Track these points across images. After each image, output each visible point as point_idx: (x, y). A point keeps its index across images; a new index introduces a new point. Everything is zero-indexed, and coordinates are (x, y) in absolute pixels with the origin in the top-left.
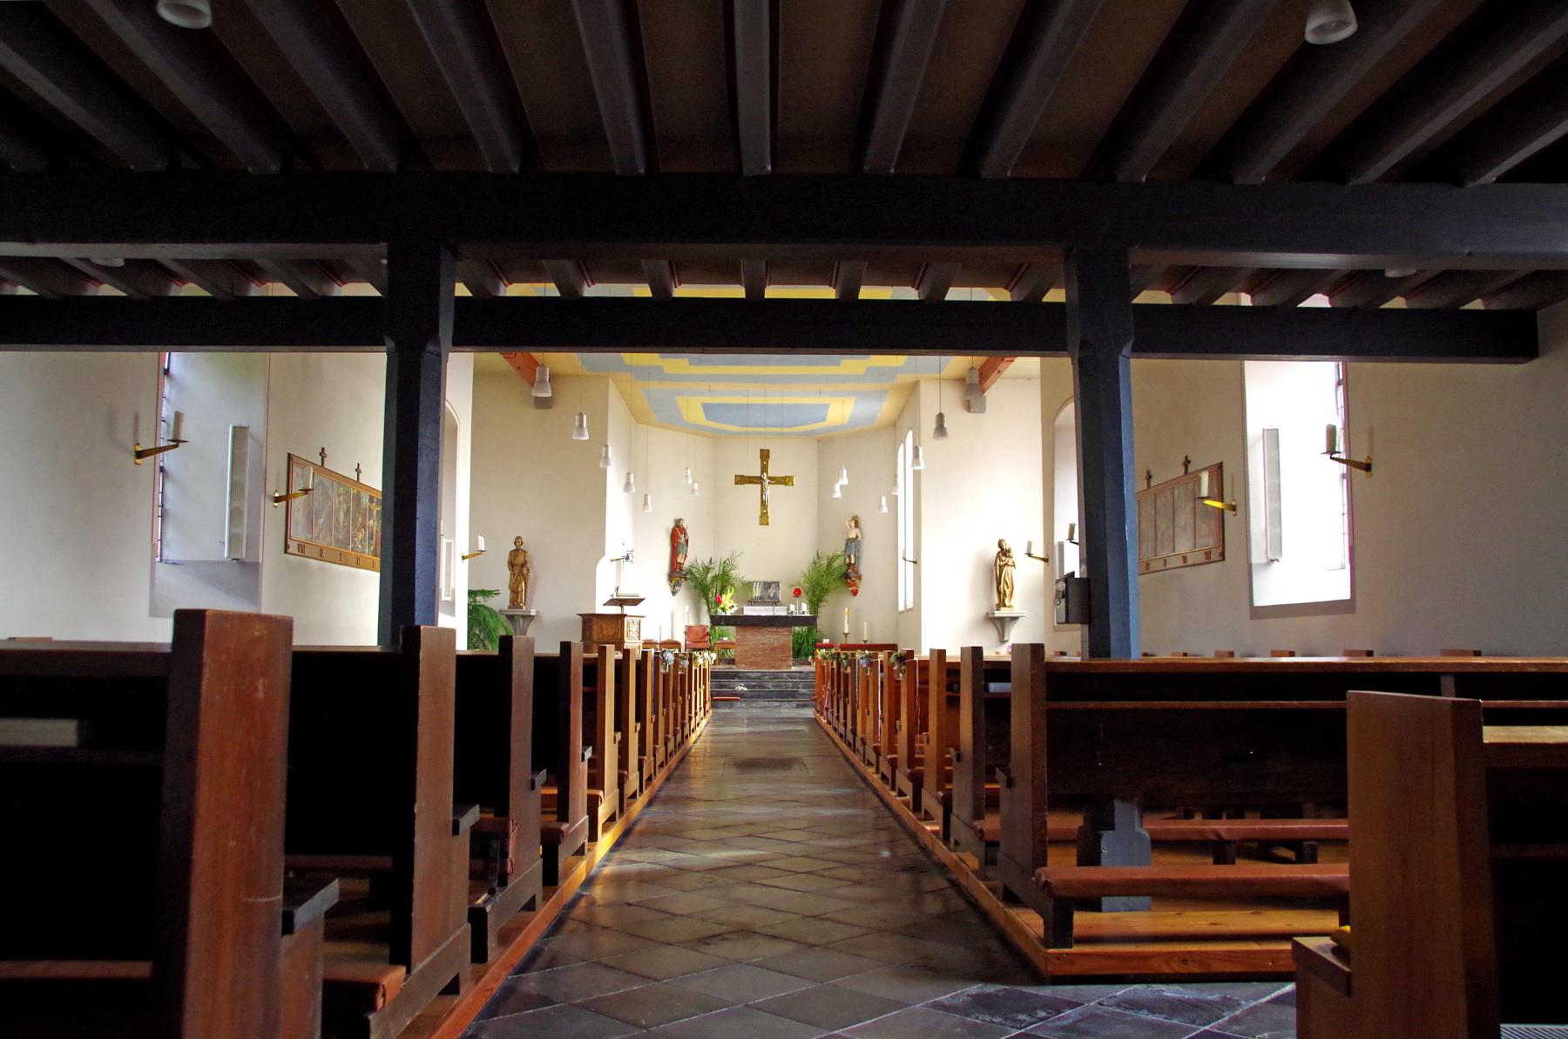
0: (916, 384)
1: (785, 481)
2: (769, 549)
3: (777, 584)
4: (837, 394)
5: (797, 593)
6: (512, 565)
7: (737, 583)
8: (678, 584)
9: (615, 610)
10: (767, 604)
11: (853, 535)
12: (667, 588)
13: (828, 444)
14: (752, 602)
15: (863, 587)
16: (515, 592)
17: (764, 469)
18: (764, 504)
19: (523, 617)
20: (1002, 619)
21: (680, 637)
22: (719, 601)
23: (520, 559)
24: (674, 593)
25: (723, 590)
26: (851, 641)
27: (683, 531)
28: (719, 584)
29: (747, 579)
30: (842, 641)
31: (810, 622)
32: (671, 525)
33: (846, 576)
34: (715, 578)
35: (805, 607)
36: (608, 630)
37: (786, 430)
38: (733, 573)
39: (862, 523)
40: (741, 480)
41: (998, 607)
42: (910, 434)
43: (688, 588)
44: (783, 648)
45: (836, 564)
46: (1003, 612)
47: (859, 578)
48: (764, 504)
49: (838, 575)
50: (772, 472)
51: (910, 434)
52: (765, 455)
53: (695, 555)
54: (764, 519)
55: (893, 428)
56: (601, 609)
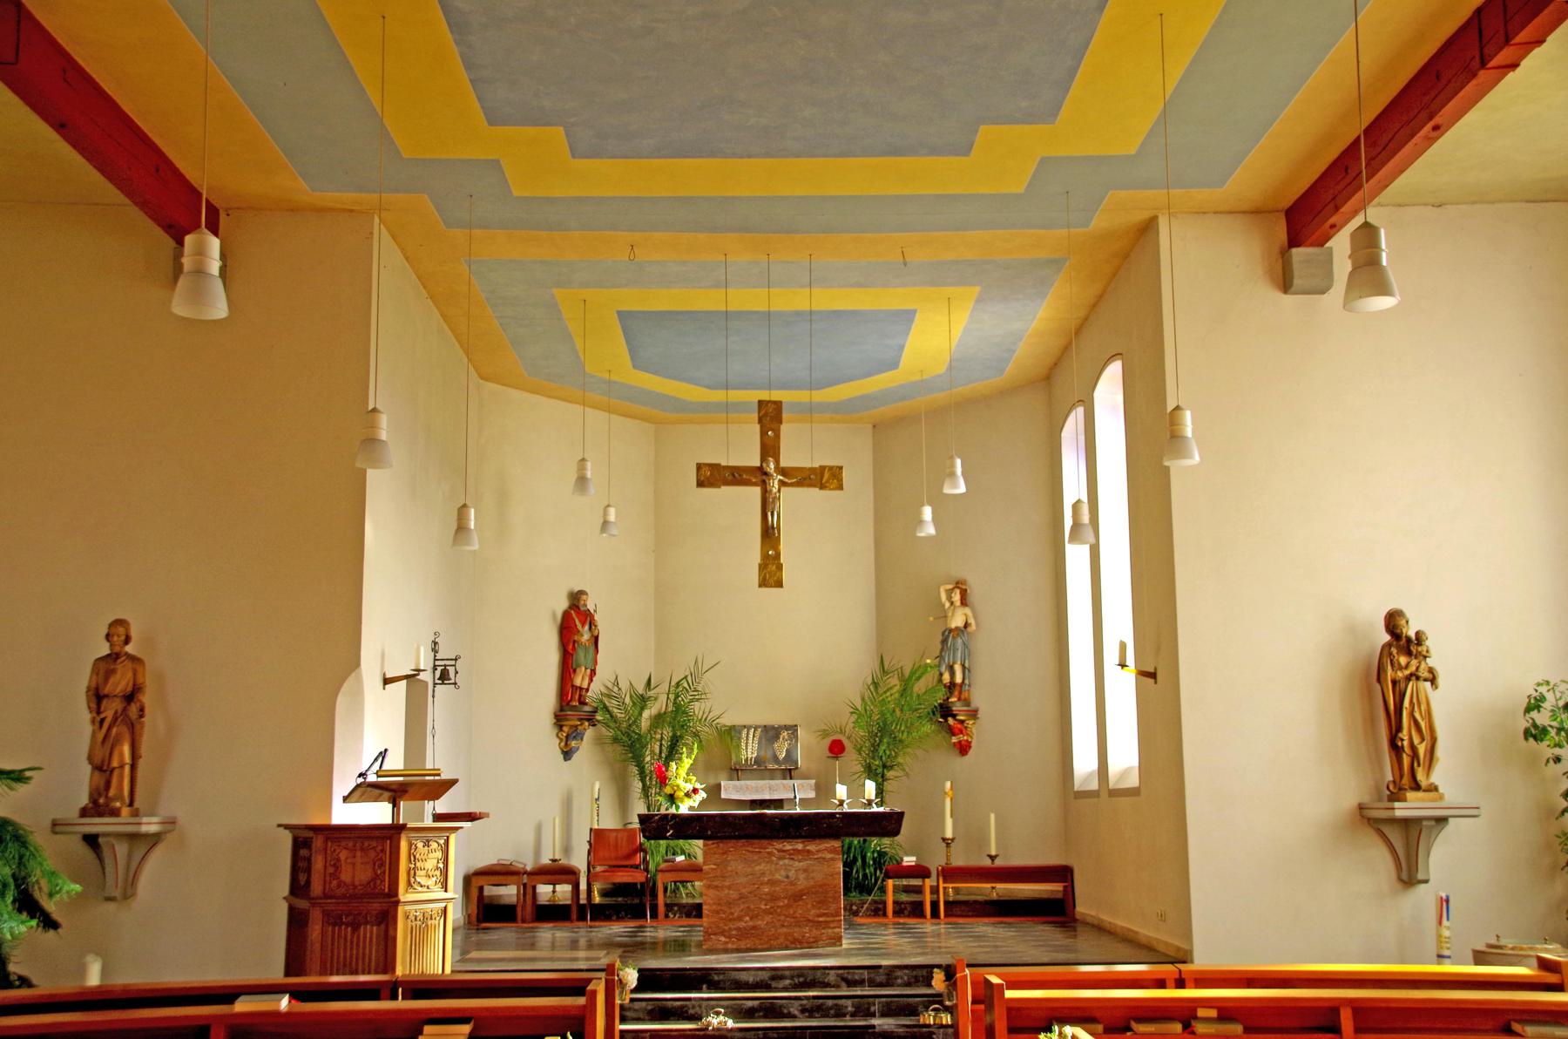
0: (1147, 228)
1: (824, 478)
2: (781, 645)
3: (793, 729)
4: (941, 275)
5: (837, 749)
6: (97, 697)
7: (705, 730)
8: (575, 734)
9: (377, 813)
10: (772, 774)
11: (957, 621)
12: (550, 743)
13: (907, 431)
14: (736, 772)
15: (977, 733)
16: (102, 768)
17: (769, 449)
18: (769, 534)
19: (134, 837)
20: (1406, 823)
21: (579, 861)
22: (663, 780)
23: (120, 682)
24: (567, 754)
25: (672, 753)
26: (958, 861)
27: (588, 618)
28: (667, 733)
29: (727, 721)
30: (935, 862)
31: (888, 824)
32: (562, 604)
33: (945, 711)
34: (658, 720)
35: (870, 787)
36: (356, 871)
37: (820, 396)
38: (697, 708)
39: (973, 596)
40: (712, 476)
41: (1396, 795)
42: (1109, 392)
43: (599, 741)
44: (820, 894)
45: (919, 687)
46: (1411, 806)
47: (974, 714)
48: (769, 534)
49: (926, 706)
50: (791, 501)
51: (1109, 392)
52: (770, 415)
53: (617, 665)
54: (770, 574)
55: (1054, 385)
56: (345, 814)
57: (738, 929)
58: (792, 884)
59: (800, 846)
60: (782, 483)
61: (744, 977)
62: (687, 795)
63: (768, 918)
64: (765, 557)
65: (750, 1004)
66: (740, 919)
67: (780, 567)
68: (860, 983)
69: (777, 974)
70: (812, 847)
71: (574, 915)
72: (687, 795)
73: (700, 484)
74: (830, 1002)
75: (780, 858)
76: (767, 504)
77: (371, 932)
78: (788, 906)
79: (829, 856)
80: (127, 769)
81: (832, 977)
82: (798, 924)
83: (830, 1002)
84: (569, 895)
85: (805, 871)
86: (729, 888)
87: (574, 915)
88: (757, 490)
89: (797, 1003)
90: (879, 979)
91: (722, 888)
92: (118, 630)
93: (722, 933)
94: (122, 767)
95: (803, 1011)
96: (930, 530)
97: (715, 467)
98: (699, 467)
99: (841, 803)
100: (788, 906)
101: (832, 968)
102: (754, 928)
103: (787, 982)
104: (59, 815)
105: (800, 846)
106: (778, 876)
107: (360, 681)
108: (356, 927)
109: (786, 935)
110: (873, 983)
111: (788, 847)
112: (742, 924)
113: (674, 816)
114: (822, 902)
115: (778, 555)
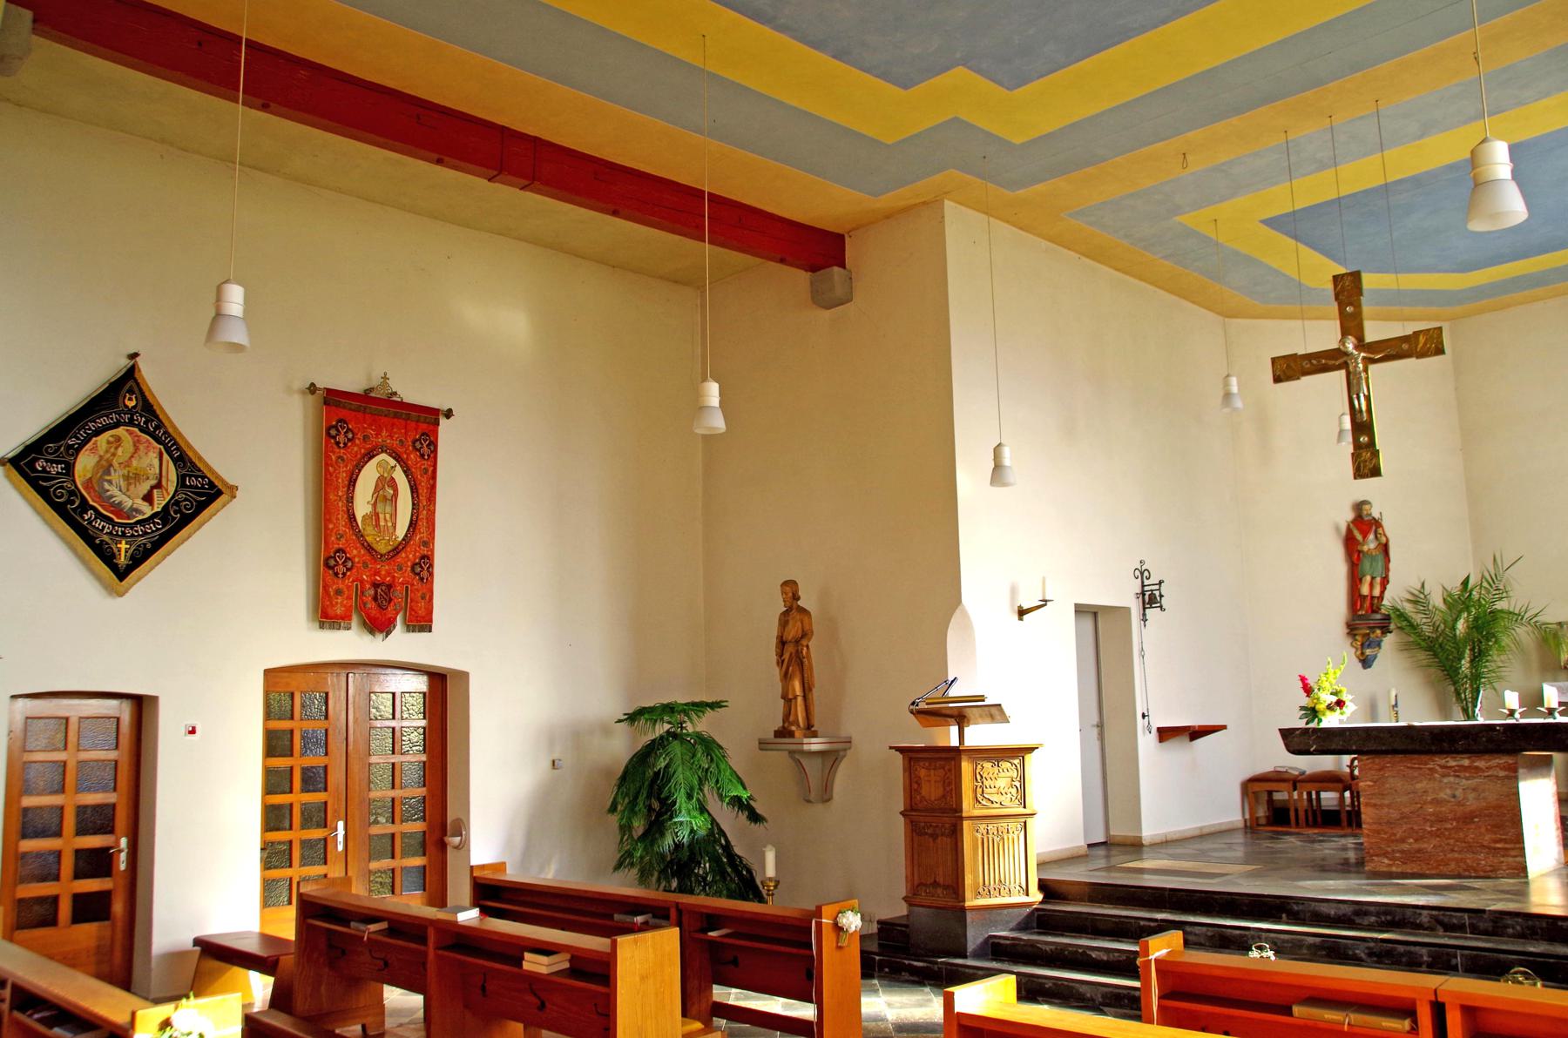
23: (792, 632)
24: (1366, 662)
40: (1288, 369)
43: (1406, 647)
52: (1348, 290)
57: (1402, 852)
58: (1459, 804)
59: (1466, 762)
60: (1369, 361)
61: (1324, 908)
62: (1329, 707)
63: (1435, 841)
64: (1357, 446)
65: (1311, 940)
66: (1403, 840)
67: (1376, 454)
68: (1460, 928)
69: (1361, 909)
70: (1480, 763)
71: (1345, 823)
72: (1329, 707)
73: (1277, 380)
74: (1401, 948)
75: (1444, 776)
76: (1352, 387)
77: (945, 841)
78: (1457, 829)
79: (1502, 774)
80: (800, 700)
81: (1425, 917)
82: (1470, 848)
83: (1401, 948)
84: (1335, 802)
85: (1474, 790)
86: (1389, 806)
87: (1345, 823)
88: (1343, 372)
89: (1363, 945)
90: (1482, 925)
91: (1382, 806)
92: (791, 590)
93: (1385, 854)
94: (795, 697)
95: (1371, 954)
96: (718, 423)
97: (1293, 357)
98: (1274, 360)
99: (1512, 713)
100: (1457, 829)
101: (1423, 907)
102: (1419, 851)
103: (1373, 919)
104: (763, 736)
105: (1466, 762)
106: (1442, 795)
107: (965, 615)
108: (934, 836)
109: (1457, 861)
110: (1475, 930)
111: (1452, 763)
112: (1405, 847)
113: (1315, 730)
114: (1498, 827)
115: (1372, 443)
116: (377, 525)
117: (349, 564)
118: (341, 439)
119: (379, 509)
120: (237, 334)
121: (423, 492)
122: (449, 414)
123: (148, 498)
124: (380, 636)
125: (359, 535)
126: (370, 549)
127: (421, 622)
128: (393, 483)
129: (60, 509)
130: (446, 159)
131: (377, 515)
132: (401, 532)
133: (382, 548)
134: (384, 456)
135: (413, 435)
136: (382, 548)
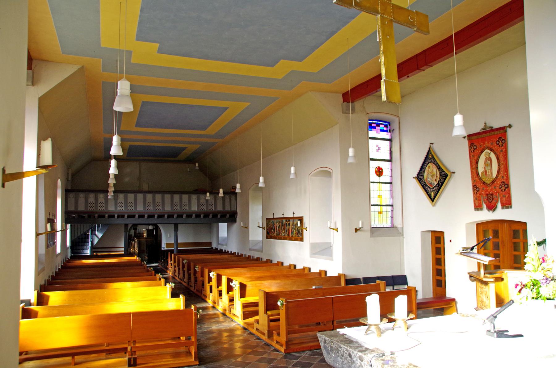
116: (486, 174)
117: (506, 186)
118: (501, 143)
119: (486, 169)
120: (350, 160)
121: (502, 158)
122: (510, 126)
123: (436, 180)
124: (491, 212)
125: (480, 179)
126: (484, 183)
127: (507, 204)
128: (490, 159)
129: (423, 186)
130: (409, 75)
131: (486, 171)
132: (494, 175)
133: (488, 182)
134: (487, 151)
135: (495, 140)
136: (488, 182)
